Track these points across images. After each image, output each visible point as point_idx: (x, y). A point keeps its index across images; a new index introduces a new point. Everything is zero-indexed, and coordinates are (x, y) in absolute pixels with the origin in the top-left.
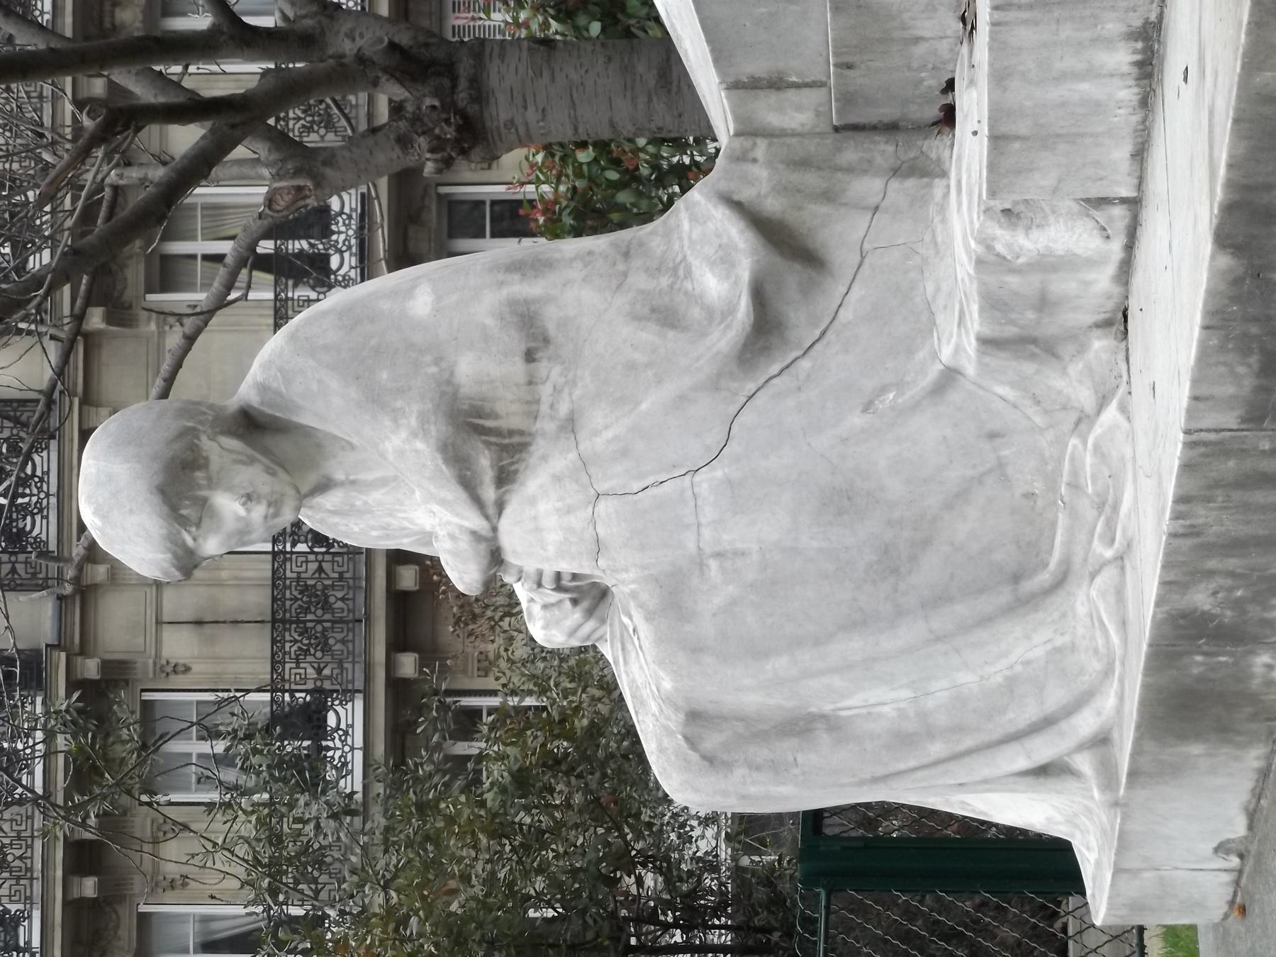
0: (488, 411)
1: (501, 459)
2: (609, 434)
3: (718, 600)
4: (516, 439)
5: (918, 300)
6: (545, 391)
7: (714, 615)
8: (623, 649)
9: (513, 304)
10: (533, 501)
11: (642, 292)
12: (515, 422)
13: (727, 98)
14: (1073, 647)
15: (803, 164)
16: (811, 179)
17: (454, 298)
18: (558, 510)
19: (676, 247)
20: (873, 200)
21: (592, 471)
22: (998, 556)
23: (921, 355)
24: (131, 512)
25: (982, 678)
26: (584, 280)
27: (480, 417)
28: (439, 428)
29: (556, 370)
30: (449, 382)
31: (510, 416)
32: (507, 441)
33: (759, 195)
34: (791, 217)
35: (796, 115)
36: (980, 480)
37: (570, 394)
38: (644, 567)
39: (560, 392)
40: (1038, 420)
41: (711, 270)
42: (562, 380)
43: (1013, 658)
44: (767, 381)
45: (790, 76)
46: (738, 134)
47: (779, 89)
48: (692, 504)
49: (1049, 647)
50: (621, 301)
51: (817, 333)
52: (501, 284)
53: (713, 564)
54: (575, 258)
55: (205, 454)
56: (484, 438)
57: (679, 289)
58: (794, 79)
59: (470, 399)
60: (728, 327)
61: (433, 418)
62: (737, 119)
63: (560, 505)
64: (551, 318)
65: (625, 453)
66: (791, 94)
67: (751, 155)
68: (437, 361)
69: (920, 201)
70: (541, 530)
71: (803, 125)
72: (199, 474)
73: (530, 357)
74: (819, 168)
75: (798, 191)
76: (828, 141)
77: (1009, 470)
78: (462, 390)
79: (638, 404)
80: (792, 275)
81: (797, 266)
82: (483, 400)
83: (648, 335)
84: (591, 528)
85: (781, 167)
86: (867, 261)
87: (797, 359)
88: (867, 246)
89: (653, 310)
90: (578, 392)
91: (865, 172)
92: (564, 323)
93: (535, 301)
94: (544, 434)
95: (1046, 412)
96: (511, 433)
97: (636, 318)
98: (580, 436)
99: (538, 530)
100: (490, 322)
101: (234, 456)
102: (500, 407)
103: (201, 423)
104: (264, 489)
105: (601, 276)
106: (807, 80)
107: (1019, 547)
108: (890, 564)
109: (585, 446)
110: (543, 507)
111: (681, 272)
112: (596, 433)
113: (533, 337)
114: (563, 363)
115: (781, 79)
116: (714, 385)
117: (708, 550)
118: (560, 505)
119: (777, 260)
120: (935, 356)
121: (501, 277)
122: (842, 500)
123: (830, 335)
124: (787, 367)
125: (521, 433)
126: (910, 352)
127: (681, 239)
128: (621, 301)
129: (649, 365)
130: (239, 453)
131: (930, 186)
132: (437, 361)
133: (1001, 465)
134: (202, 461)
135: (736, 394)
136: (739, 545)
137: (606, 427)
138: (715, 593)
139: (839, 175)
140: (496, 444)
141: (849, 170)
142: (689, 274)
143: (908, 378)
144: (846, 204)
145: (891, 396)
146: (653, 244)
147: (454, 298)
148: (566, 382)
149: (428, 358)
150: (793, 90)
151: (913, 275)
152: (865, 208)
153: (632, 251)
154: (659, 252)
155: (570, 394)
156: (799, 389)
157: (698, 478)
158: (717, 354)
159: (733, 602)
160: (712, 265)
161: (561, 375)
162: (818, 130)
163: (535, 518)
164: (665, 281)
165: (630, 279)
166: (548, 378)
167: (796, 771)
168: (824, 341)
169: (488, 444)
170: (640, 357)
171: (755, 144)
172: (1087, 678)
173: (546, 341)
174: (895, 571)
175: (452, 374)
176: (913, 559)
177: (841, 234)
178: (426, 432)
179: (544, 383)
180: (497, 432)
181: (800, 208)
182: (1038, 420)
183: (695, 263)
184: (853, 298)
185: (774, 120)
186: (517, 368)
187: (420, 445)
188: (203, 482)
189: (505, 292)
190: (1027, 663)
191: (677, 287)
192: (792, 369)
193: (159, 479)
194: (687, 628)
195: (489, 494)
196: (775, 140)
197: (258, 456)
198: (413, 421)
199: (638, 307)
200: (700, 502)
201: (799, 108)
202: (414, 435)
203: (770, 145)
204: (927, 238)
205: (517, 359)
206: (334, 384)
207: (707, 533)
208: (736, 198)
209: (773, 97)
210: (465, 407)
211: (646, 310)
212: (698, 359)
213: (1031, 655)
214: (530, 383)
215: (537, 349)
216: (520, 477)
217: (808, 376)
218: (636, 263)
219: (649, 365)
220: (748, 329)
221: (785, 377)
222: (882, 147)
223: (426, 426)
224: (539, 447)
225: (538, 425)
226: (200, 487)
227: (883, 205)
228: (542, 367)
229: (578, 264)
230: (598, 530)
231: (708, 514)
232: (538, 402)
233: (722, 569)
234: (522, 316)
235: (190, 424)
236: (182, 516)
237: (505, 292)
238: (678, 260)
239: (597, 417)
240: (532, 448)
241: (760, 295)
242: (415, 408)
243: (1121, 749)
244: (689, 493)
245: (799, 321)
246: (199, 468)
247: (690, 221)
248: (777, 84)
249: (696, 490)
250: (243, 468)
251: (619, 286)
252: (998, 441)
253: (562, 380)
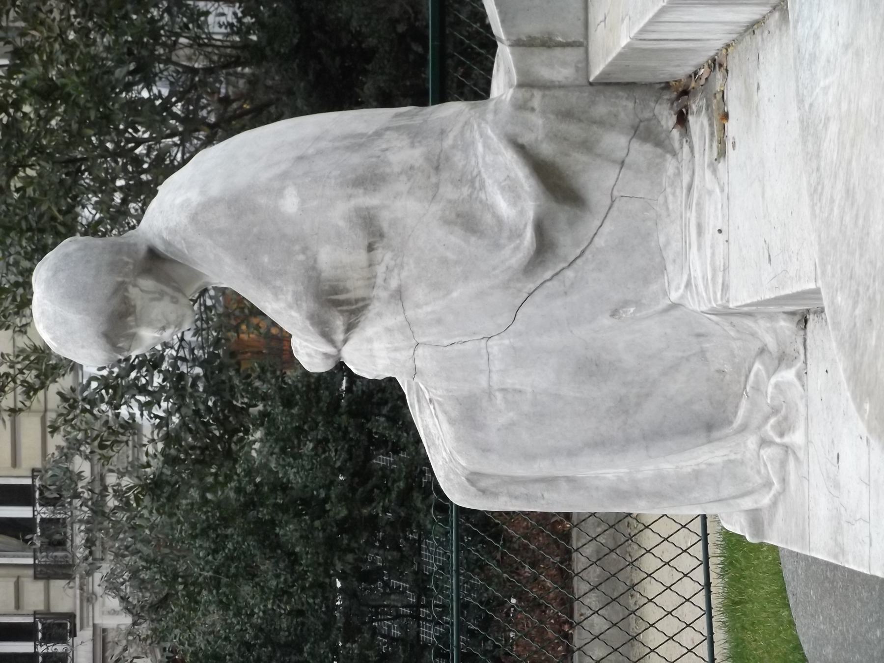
0: (341, 288)
1: (350, 319)
2: (429, 309)
3: (502, 420)
4: (361, 304)
5: (653, 244)
6: (381, 270)
7: (499, 430)
8: (419, 401)
9: (358, 210)
10: (370, 341)
11: (450, 201)
12: (360, 293)
13: (512, 53)
14: (742, 462)
15: (567, 115)
16: (574, 130)
17: (315, 203)
18: (388, 348)
19: (473, 163)
20: (620, 154)
21: (414, 329)
22: (697, 407)
23: (654, 287)
24: (83, 347)
25: (677, 467)
26: (408, 192)
27: (336, 294)
28: (308, 305)
29: (388, 256)
30: (314, 268)
31: (356, 289)
32: (354, 307)
33: (536, 139)
34: (560, 161)
35: (562, 70)
36: (687, 359)
37: (399, 275)
38: (447, 390)
39: (392, 270)
40: (732, 333)
41: (502, 194)
42: (392, 263)
43: (700, 460)
44: (542, 284)
45: (557, 36)
46: (520, 85)
47: (549, 47)
48: (486, 357)
49: (726, 458)
50: (436, 208)
51: (578, 251)
52: (350, 196)
53: (499, 395)
54: (401, 173)
55: (133, 303)
56: (339, 308)
57: (476, 198)
58: (560, 39)
59: (329, 281)
60: (517, 248)
61: (304, 298)
62: (520, 72)
63: (390, 346)
64: (385, 219)
65: (439, 321)
66: (558, 52)
67: (530, 104)
68: (304, 250)
69: (656, 168)
70: (374, 357)
71: (566, 78)
72: (130, 319)
73: (370, 248)
74: (580, 120)
75: (565, 139)
76: (586, 94)
77: (708, 355)
78: (323, 275)
79: (449, 292)
80: (563, 213)
81: (567, 208)
82: (338, 280)
83: (456, 238)
84: (411, 361)
85: (552, 117)
86: (616, 205)
87: (563, 269)
88: (615, 193)
89: (458, 215)
90: (404, 274)
91: (612, 126)
92: (394, 223)
93: (373, 208)
94: (379, 299)
95: (738, 331)
96: (357, 301)
97: (446, 222)
98: (407, 304)
99: (372, 356)
100: (341, 223)
101: (151, 296)
102: (349, 284)
103: (126, 275)
104: (172, 317)
105: (420, 188)
106: (569, 40)
107: (712, 403)
108: (623, 407)
109: (410, 313)
110: (376, 345)
111: (477, 184)
112: (418, 306)
113: (372, 234)
114: (393, 251)
115: (550, 39)
116: (506, 286)
117: (496, 387)
118: (390, 346)
119: (554, 205)
120: (665, 294)
121: (350, 191)
122: (592, 367)
123: (587, 253)
124: (557, 274)
125: (364, 299)
126: (646, 282)
127: (476, 156)
128: (436, 208)
129: (457, 262)
130: (154, 292)
131: (662, 157)
132: (304, 250)
133: (703, 352)
134: (132, 310)
135: (520, 291)
136: (518, 387)
137: (426, 304)
138: (499, 416)
139: (595, 128)
140: (347, 311)
141: (600, 123)
142: (483, 187)
143: (644, 301)
144: (599, 156)
145: (632, 310)
146: (456, 159)
147: (315, 203)
148: (396, 265)
149: (297, 248)
150: (559, 49)
151: (649, 224)
152: (614, 161)
153: (441, 166)
154: (460, 165)
155: (399, 275)
156: (566, 293)
157: (490, 343)
158: (509, 268)
159: (512, 424)
160: (503, 189)
161: (392, 259)
162: (577, 82)
163: (371, 350)
164: (466, 191)
165: (441, 190)
166: (382, 260)
167: (543, 502)
168: (583, 258)
169: (342, 312)
170: (450, 255)
171: (533, 95)
172: (751, 485)
173: (382, 236)
174: (626, 412)
175: (315, 261)
176: (638, 404)
177: (597, 181)
178: (299, 307)
179: (379, 264)
180: (348, 302)
181: (567, 155)
182: (732, 333)
183: (489, 182)
184: (604, 230)
185: (546, 73)
186: (362, 257)
187: (294, 314)
188: (133, 324)
189: (353, 203)
190: (710, 464)
191: (474, 196)
192: (560, 277)
193: (103, 328)
194: (480, 435)
195: (339, 337)
196: (547, 92)
197: (165, 288)
198: (290, 298)
199: (447, 213)
200: (491, 357)
201: (564, 64)
202: (290, 307)
203: (544, 96)
204: (661, 199)
205: (362, 251)
206: (228, 260)
207: (495, 377)
208: (520, 141)
209: (544, 54)
210: (327, 288)
211: (453, 215)
212: (494, 269)
213: (712, 461)
214: (370, 265)
215: (375, 242)
216: (361, 325)
217: (572, 284)
218: (445, 175)
219: (457, 262)
220: (532, 253)
221: (555, 282)
222: (624, 102)
223: (299, 302)
224: (375, 307)
225: (375, 292)
226: (131, 327)
227: (627, 161)
228: (379, 253)
229: (403, 178)
230: (417, 363)
231: (497, 366)
232: (375, 277)
233: (505, 399)
234: (364, 218)
235: (120, 279)
236: (120, 348)
237: (353, 203)
238: (475, 173)
239: (419, 293)
240: (370, 307)
241: (540, 230)
242: (291, 288)
243: (708, 224)
244: (484, 351)
245: (566, 243)
246: (130, 314)
247: (484, 146)
248: (547, 43)
249: (490, 350)
250: (156, 303)
251: (434, 197)
252: (701, 339)
253: (392, 263)
